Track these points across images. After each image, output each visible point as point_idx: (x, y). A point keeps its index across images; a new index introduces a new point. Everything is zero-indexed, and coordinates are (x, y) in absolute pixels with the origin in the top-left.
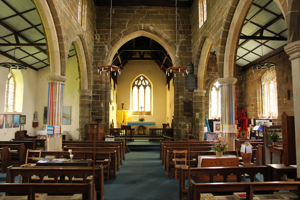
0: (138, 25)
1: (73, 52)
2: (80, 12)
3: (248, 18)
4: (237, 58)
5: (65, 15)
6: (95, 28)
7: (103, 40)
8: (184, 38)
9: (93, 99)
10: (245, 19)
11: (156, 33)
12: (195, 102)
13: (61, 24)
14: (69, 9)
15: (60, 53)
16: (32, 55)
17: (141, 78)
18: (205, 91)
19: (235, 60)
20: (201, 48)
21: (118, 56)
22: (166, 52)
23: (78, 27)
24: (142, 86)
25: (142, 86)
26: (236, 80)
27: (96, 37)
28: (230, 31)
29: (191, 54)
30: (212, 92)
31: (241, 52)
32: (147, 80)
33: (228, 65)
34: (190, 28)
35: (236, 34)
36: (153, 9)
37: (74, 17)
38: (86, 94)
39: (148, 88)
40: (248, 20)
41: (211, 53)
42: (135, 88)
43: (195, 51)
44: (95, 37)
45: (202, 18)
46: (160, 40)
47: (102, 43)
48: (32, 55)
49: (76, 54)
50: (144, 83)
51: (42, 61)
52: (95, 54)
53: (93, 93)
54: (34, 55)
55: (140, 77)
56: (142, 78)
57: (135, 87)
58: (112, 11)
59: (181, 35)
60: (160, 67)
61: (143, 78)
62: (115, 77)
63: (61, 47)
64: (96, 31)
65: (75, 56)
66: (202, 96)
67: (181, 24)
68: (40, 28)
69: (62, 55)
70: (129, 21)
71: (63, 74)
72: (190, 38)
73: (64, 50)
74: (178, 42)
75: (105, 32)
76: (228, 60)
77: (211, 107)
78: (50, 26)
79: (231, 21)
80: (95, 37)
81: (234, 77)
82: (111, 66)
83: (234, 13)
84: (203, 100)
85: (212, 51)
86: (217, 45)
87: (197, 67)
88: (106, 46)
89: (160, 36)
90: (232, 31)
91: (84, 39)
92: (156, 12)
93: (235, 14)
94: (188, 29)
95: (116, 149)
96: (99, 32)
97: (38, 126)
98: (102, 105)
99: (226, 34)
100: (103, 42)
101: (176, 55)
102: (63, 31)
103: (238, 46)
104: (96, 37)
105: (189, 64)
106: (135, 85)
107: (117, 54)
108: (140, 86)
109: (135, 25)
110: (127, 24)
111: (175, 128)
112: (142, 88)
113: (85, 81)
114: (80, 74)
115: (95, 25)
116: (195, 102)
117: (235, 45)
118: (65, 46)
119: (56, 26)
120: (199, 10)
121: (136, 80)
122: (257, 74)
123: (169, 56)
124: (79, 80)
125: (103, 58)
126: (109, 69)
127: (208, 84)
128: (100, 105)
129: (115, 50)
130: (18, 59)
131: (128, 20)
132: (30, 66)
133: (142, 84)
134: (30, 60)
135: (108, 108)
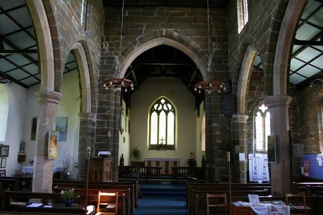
0: (158, 30)
1: (73, 65)
2: (84, 14)
3: (304, 17)
4: (291, 72)
5: (64, 14)
6: (103, 33)
7: (113, 50)
8: (218, 47)
9: (97, 126)
10: (300, 19)
11: (181, 41)
12: (234, 132)
13: (57, 24)
14: (69, 7)
15: (55, 61)
16: (21, 68)
17: (161, 101)
18: (247, 117)
19: (289, 75)
20: (242, 59)
21: (133, 71)
22: (194, 65)
23: (80, 31)
24: (163, 111)
25: (163, 111)
26: (290, 99)
27: (104, 45)
28: (280, 33)
29: (228, 68)
30: (257, 118)
31: (295, 64)
32: (170, 104)
33: (279, 79)
34: (227, 35)
35: (288, 36)
36: (177, 11)
37: (75, 17)
38: (89, 118)
39: (171, 114)
40: (304, 21)
41: (254, 66)
42: (154, 114)
43: (232, 63)
44: (102, 46)
45: (242, 21)
46: (188, 49)
47: (111, 53)
48: (21, 68)
49: (77, 68)
50: (165, 108)
51: (33, 76)
52: (102, 66)
53: (97, 118)
54: (23, 68)
55: (161, 99)
56: (163, 101)
57: (154, 112)
58: (125, 13)
59: (214, 44)
60: (187, 87)
61: (164, 101)
62: (127, 96)
63: (56, 53)
64: (104, 37)
65: (77, 70)
66: (243, 123)
67: (214, 30)
68: (31, 30)
69: (57, 65)
70: (146, 25)
71: (57, 89)
72: (227, 47)
73: (60, 58)
74: (211, 51)
75: (116, 39)
76: (279, 71)
77: (255, 138)
78: (42, 26)
79: (282, 20)
80: (102, 46)
81: (288, 94)
82: (122, 80)
83: (285, 9)
84: (244, 128)
85: (256, 64)
86: (264, 52)
87: (236, 84)
88: (117, 57)
89: (187, 44)
90: (283, 34)
91: (87, 47)
92: (182, 14)
93: (287, 9)
94: (224, 36)
95: (125, 192)
96: (107, 40)
97: (24, 161)
98: (109, 134)
99: (275, 37)
100: (112, 52)
101: (208, 69)
102: (59, 33)
103: (292, 55)
104: (104, 45)
105: (225, 81)
106: (154, 110)
107: (131, 67)
108: (160, 111)
109: (154, 30)
110: (144, 29)
111: (207, 166)
112: (163, 114)
113: (88, 101)
114: (81, 92)
115: (103, 31)
116: (234, 132)
117: (290, 41)
118: (61, 53)
119: (50, 27)
120: (238, 11)
121: (155, 104)
122: (318, 94)
123: (198, 71)
124: (79, 102)
125: (112, 73)
126: (120, 83)
127: (252, 108)
128: (107, 133)
129: (128, 63)
130: (4, 71)
131: (145, 25)
132: (18, 82)
133: (163, 109)
134: (18, 74)
135: (118, 138)
